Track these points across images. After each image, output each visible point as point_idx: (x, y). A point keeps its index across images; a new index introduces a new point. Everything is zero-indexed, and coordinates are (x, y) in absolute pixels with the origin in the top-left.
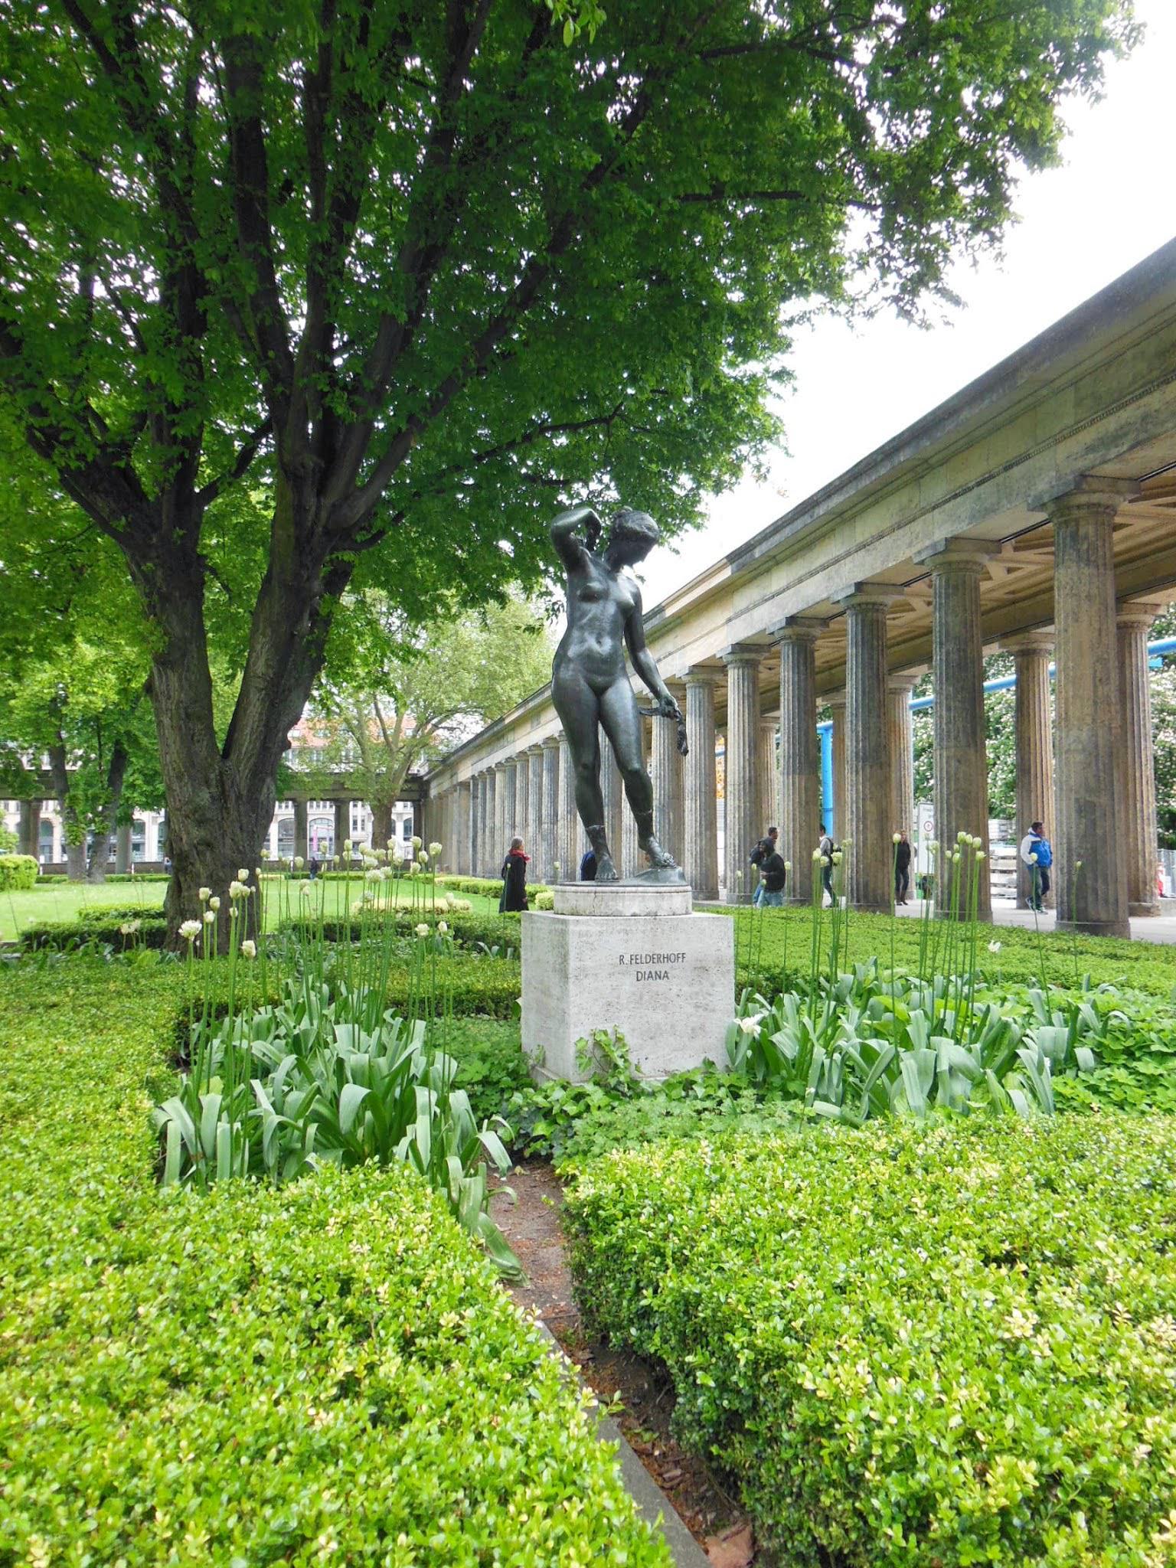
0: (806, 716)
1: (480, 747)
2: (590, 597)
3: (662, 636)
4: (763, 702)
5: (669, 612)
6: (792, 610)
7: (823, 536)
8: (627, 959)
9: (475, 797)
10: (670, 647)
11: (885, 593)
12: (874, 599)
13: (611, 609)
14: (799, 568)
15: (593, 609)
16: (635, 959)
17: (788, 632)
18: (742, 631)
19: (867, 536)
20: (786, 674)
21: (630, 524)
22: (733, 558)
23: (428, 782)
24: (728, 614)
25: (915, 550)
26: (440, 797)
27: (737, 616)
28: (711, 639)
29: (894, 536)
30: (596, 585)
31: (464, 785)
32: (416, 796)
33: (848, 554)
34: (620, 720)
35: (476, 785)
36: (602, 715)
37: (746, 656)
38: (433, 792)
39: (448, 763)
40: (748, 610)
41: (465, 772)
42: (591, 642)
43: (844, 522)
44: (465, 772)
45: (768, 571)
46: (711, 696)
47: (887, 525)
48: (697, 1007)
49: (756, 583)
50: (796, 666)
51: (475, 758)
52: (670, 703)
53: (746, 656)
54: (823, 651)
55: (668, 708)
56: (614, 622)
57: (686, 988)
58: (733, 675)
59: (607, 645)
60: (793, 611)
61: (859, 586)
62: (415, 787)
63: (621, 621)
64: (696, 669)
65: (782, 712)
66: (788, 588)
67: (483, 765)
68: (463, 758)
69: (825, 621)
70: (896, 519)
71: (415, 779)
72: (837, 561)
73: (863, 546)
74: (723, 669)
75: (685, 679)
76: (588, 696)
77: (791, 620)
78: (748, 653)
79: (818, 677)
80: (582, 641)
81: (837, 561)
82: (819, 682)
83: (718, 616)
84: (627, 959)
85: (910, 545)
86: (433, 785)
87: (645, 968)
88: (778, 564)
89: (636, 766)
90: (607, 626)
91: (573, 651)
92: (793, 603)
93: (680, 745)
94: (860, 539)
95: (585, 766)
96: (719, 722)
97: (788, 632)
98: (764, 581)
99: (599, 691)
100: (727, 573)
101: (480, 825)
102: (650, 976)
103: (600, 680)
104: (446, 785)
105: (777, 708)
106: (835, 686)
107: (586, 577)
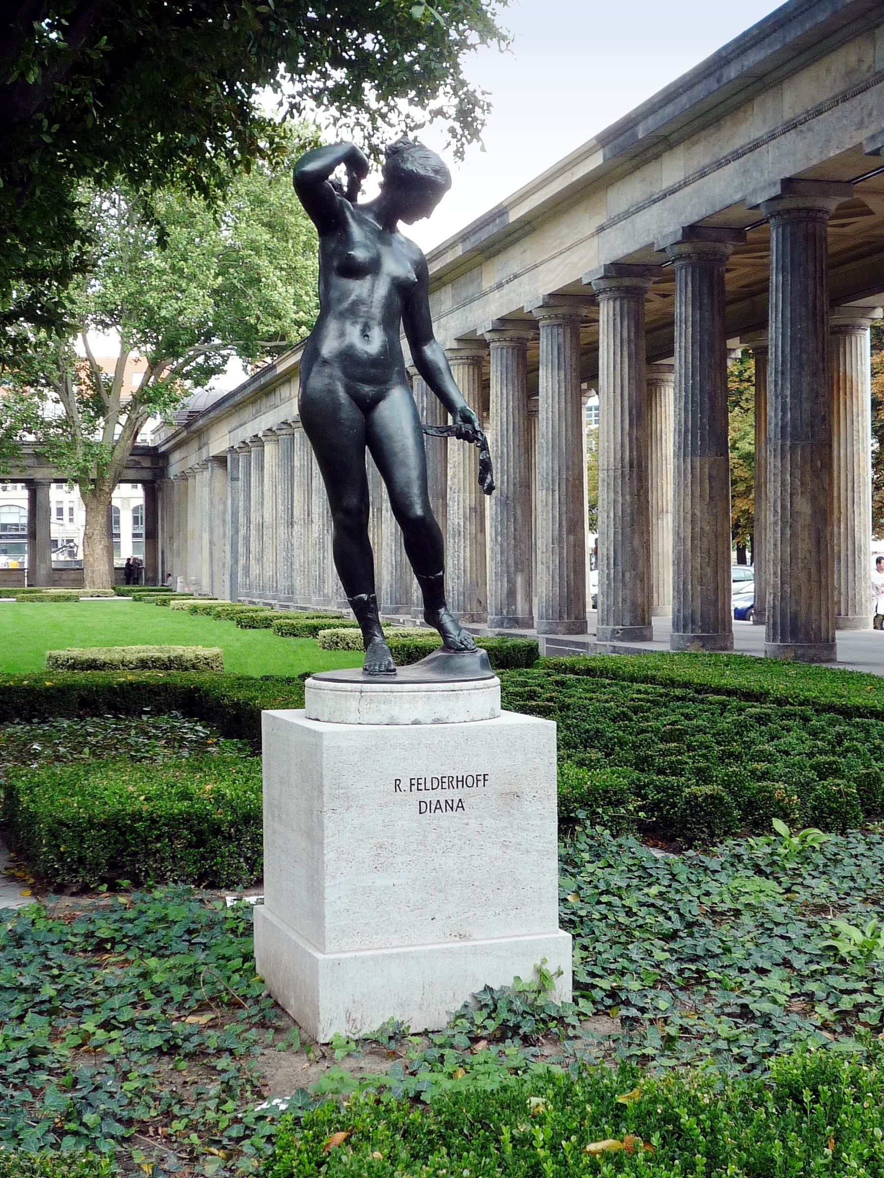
0: (711, 360)
1: (239, 407)
3: (514, 242)
4: (651, 346)
5: (514, 216)
6: (692, 215)
7: (737, 107)
8: (405, 785)
9: (235, 479)
10: (515, 267)
11: (826, 194)
12: (808, 203)
14: (699, 154)
15: (358, 288)
16: (416, 784)
17: (686, 248)
18: (620, 244)
19: (799, 110)
20: (683, 310)
21: (409, 166)
22: (605, 139)
23: (165, 456)
24: (600, 220)
25: (867, 133)
26: (184, 477)
27: (613, 222)
29: (838, 111)
30: (360, 254)
31: (221, 460)
32: (146, 475)
33: (773, 137)
34: (397, 446)
35: (236, 462)
36: (373, 438)
37: (626, 282)
38: (174, 470)
39: (193, 428)
40: (627, 215)
41: (220, 441)
42: (353, 334)
43: (766, 88)
45: (657, 156)
46: (575, 335)
47: (825, 95)
48: (505, 845)
49: (638, 174)
50: (697, 302)
51: (234, 421)
52: (467, 419)
53: (626, 282)
54: (737, 273)
56: (388, 306)
57: (488, 822)
58: (606, 311)
60: (694, 218)
61: (788, 184)
62: (146, 463)
63: (398, 301)
64: (556, 299)
65: (675, 360)
66: (686, 184)
67: (247, 433)
68: (218, 420)
69: (738, 233)
70: (840, 87)
71: (151, 453)
72: (756, 146)
73: (792, 126)
74: (591, 300)
75: (537, 314)
76: (348, 410)
77: (692, 232)
78: (629, 277)
79: (729, 309)
80: (342, 334)
81: (756, 146)
82: (734, 313)
83: (584, 222)
84: (405, 785)
85: (860, 125)
86: (175, 457)
87: (430, 796)
88: (671, 147)
89: (419, 511)
90: (377, 311)
91: (329, 347)
92: (691, 207)
93: (482, 481)
94: (788, 115)
95: (347, 512)
97: (686, 248)
98: (650, 170)
99: (368, 406)
100: (597, 161)
101: (242, 520)
102: (438, 807)
103: (367, 389)
104: (193, 460)
105: (670, 353)
106: (753, 325)
107: (347, 240)
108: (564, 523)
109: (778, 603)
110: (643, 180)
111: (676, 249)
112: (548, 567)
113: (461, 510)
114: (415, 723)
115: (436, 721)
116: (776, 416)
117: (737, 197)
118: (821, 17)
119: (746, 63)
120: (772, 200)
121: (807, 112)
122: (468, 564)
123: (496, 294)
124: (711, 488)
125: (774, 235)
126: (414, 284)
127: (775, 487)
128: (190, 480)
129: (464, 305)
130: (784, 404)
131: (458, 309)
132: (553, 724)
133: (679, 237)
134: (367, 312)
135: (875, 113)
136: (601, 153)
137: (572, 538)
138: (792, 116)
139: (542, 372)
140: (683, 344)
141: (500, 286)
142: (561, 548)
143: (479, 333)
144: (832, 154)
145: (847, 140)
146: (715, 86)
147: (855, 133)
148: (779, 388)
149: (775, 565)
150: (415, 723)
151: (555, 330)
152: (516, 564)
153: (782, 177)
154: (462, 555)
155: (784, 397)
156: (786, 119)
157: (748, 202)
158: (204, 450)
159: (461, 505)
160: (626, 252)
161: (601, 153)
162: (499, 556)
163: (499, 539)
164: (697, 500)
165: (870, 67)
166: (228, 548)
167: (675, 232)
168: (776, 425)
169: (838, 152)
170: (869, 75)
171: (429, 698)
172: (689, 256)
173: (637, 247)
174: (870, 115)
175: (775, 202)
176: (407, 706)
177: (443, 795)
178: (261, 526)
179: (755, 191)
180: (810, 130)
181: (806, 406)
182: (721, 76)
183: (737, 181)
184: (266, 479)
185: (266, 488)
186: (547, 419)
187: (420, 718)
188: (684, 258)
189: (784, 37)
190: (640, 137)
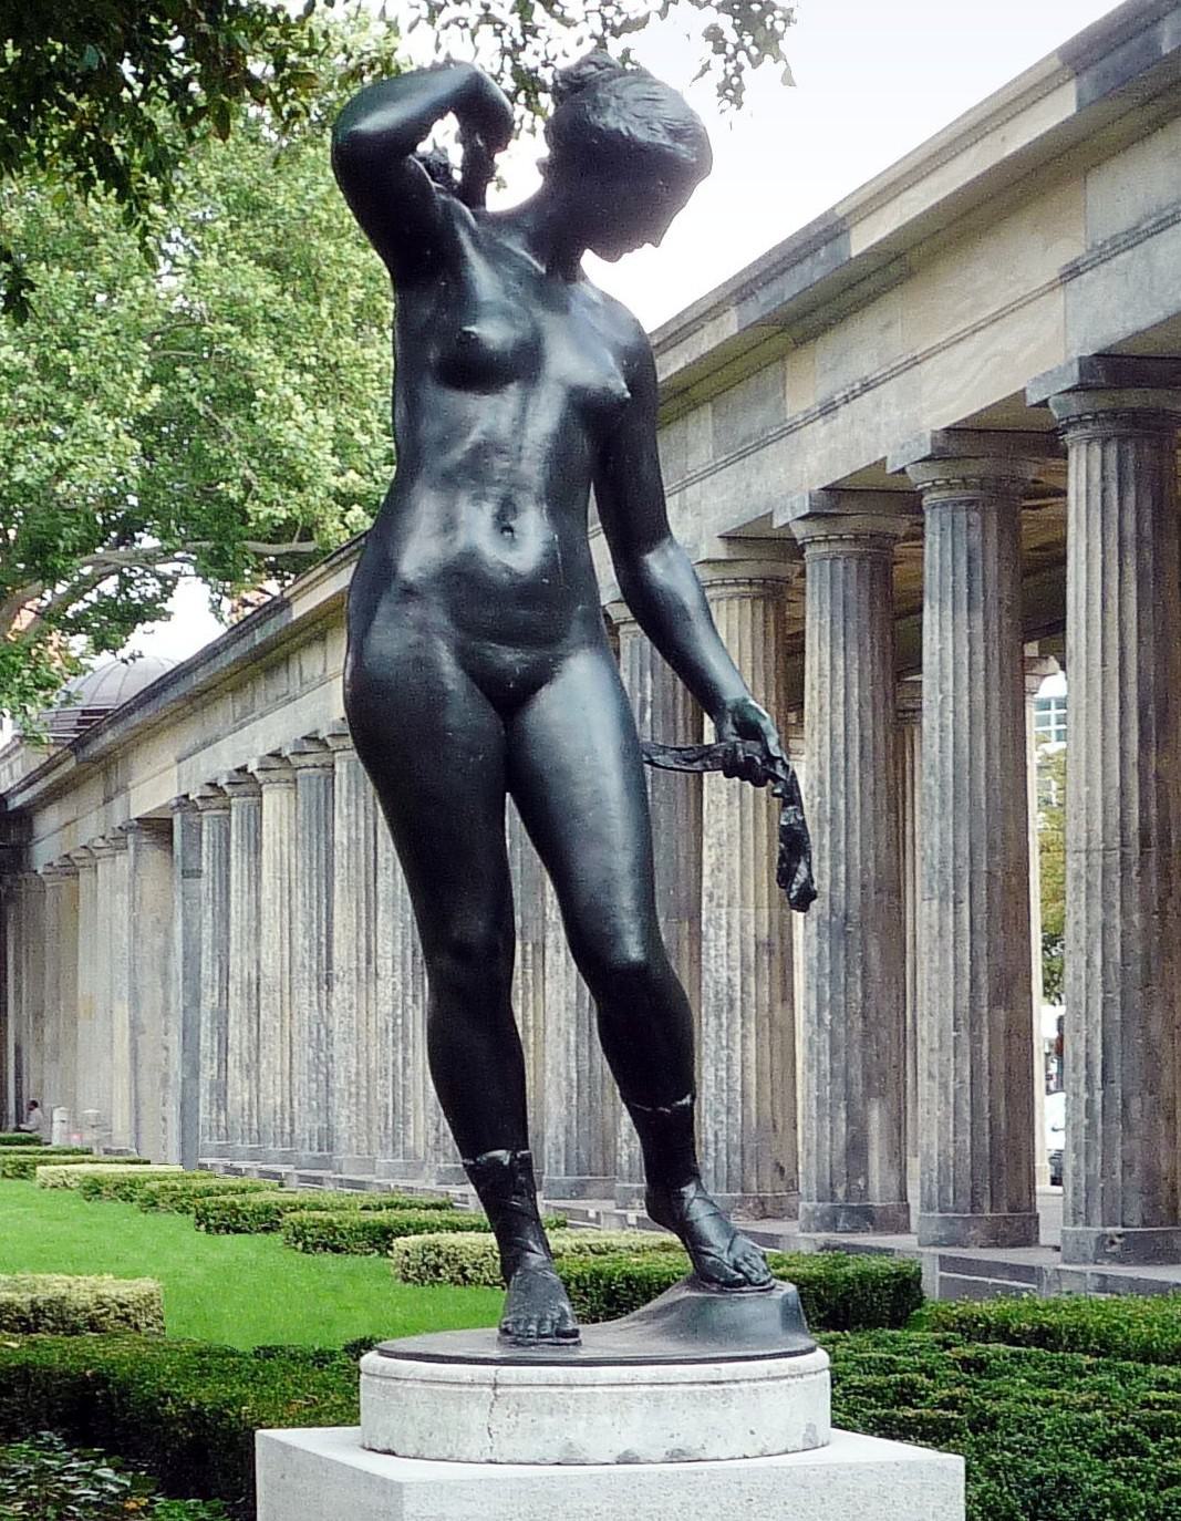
2: (477, 371)
5: (863, 239)
10: (864, 364)
13: (545, 416)
23: (25, 817)
24: (1070, 249)
27: (1102, 254)
28: (1006, 339)
30: (492, 332)
31: (158, 828)
34: (582, 795)
36: (523, 776)
37: (1133, 399)
41: (154, 785)
42: (477, 527)
44: (154, 785)
46: (1010, 527)
51: (190, 735)
53: (1133, 399)
55: (747, 749)
56: (559, 455)
59: (526, 549)
63: (583, 446)
67: (220, 761)
74: (1049, 443)
75: (919, 477)
80: (449, 525)
83: (1030, 256)
89: (634, 951)
90: (533, 469)
91: (418, 556)
93: (785, 877)
95: (461, 952)
96: (1036, 619)
99: (511, 698)
100: (1062, 107)
101: (208, 971)
103: (510, 658)
107: (461, 299)
113: (737, 947)
114: (626, 1459)
115: (676, 1457)
122: (752, 1078)
123: (820, 428)
126: (623, 403)
128: (84, 877)
129: (743, 455)
131: (727, 464)
132: (956, 1463)
134: (510, 471)
141: (828, 409)
143: (778, 522)
150: (626, 1459)
152: (868, 1078)
154: (737, 1056)
158: (117, 803)
159: (736, 937)
162: (826, 1059)
163: (827, 1017)
166: (175, 1040)
171: (658, 1400)
176: (607, 1419)
178: (255, 988)
184: (266, 875)
185: (266, 895)
186: (942, 728)
187: (637, 1448)
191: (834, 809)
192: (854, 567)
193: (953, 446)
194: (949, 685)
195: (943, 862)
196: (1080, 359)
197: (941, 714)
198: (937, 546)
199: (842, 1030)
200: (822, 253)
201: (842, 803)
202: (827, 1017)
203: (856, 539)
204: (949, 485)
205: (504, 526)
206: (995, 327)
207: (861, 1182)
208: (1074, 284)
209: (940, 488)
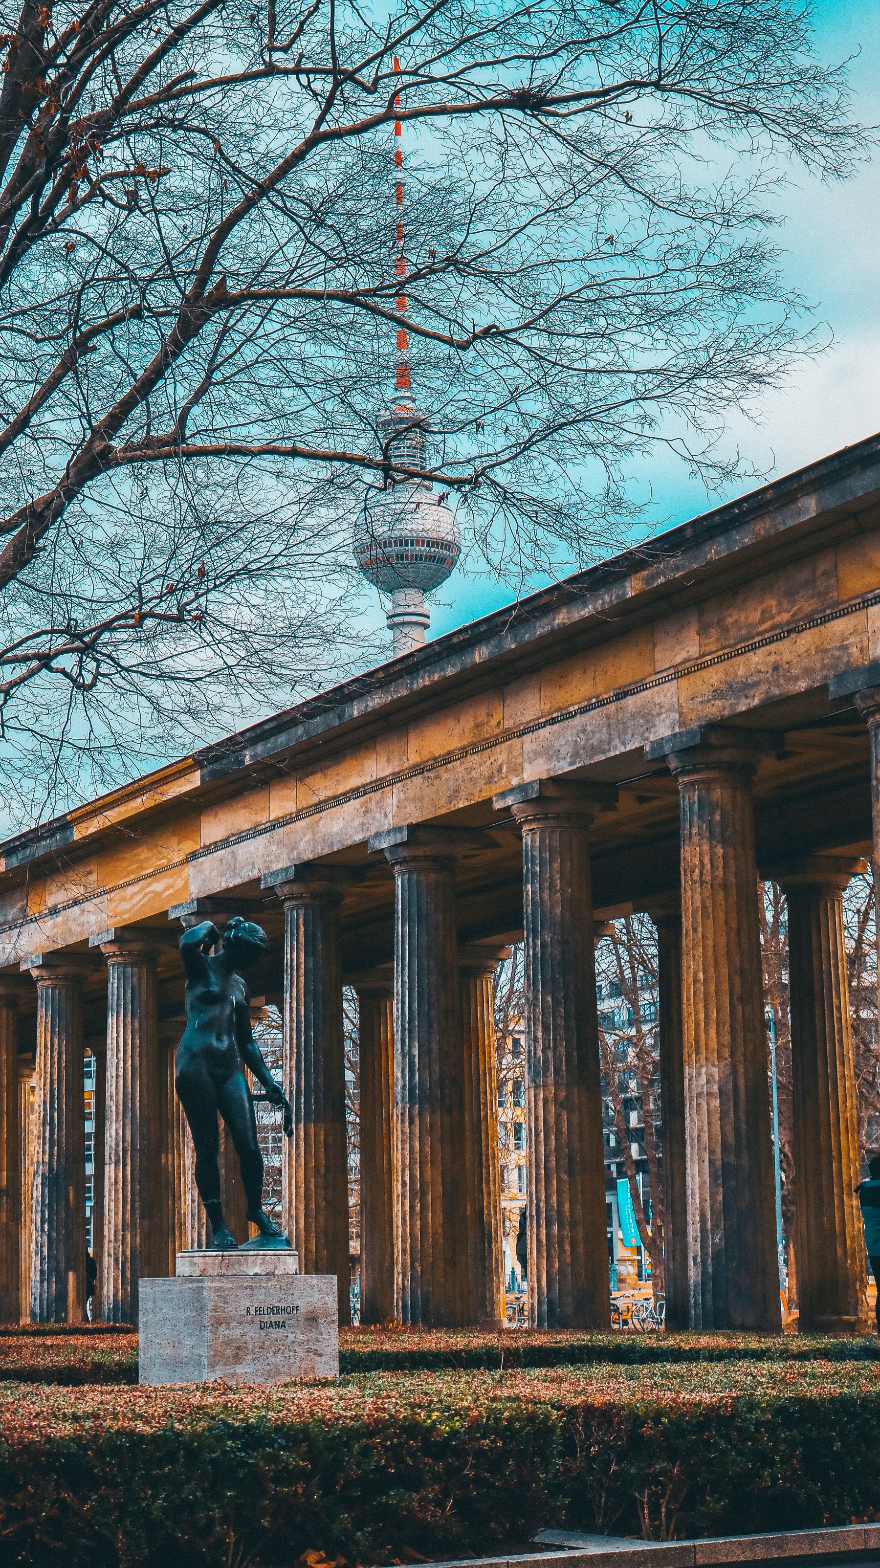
5: (79, 833)
6: (307, 851)
17: (295, 888)
100: (194, 781)
108: (137, 1204)
109: (408, 1284)
110: (245, 807)
111: (287, 889)
112: (116, 1260)
116: (403, 1078)
117: (358, 838)
118: (450, 671)
119: (371, 704)
120: (397, 845)
121: (435, 759)
124: (327, 1157)
125: (399, 883)
127: (403, 1155)
130: (412, 1064)
133: (291, 875)
135: (504, 770)
136: (198, 774)
137: (146, 1223)
138: (419, 760)
139: (111, 1021)
140: (294, 994)
142: (180, 1218)
143: (23, 967)
144: (461, 805)
145: (477, 794)
146: (336, 723)
147: (484, 787)
148: (406, 1048)
149: (404, 1241)
151: (129, 970)
152: (68, 1260)
153: (408, 822)
155: (411, 1057)
156: (411, 762)
157: (370, 846)
160: (224, 886)
161: (198, 774)
164: (311, 1173)
165: (499, 723)
167: (286, 869)
168: (404, 1087)
169: (467, 804)
170: (498, 731)
172: (300, 897)
173: (238, 881)
174: (500, 770)
175: (401, 849)
177: (273, 1318)
179: (378, 835)
180: (437, 777)
181: (436, 1068)
182: (343, 711)
183: (358, 822)
186: (117, 1076)
188: (297, 898)
189: (412, 683)
190: (247, 763)
191: (52, 1117)
192: (64, 992)
193: (127, 935)
194: (121, 1055)
195: (117, 1145)
196: (198, 899)
197: (117, 1069)
198: (115, 985)
199: (54, 1234)
200: (58, 836)
201: (56, 1115)
202: (46, 1227)
203: (57, 978)
204: (121, 955)
205: (219, 1039)
206: (149, 880)
207: (649, 1229)
208: (194, 863)
209: (117, 956)
